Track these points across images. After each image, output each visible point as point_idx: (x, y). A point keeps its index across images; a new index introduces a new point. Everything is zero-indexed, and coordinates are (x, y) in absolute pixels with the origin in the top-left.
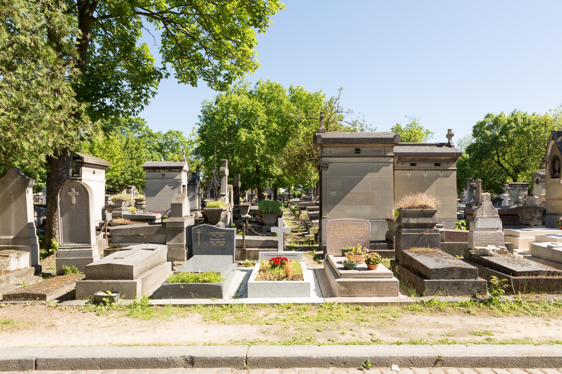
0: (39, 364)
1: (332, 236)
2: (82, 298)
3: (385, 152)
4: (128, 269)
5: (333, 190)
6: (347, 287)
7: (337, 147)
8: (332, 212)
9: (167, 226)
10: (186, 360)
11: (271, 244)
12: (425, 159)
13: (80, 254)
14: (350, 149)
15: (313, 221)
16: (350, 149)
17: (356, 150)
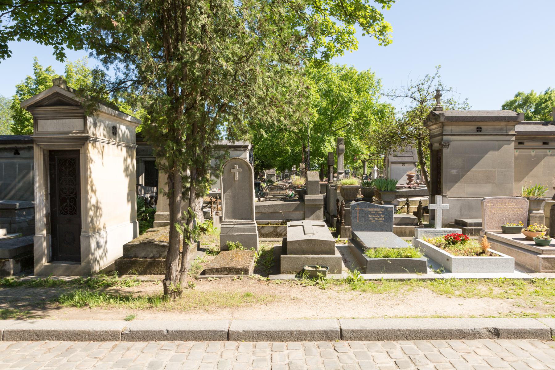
0: (345, 334)
1: (489, 214)
2: (288, 272)
3: (507, 131)
4: (330, 244)
5: (454, 169)
6: (551, 263)
7: (459, 125)
8: (452, 190)
9: (306, 203)
10: (490, 331)
11: (407, 221)
12: (534, 138)
13: (244, 230)
14: (472, 128)
15: (399, 200)
16: (472, 128)
17: (477, 128)
